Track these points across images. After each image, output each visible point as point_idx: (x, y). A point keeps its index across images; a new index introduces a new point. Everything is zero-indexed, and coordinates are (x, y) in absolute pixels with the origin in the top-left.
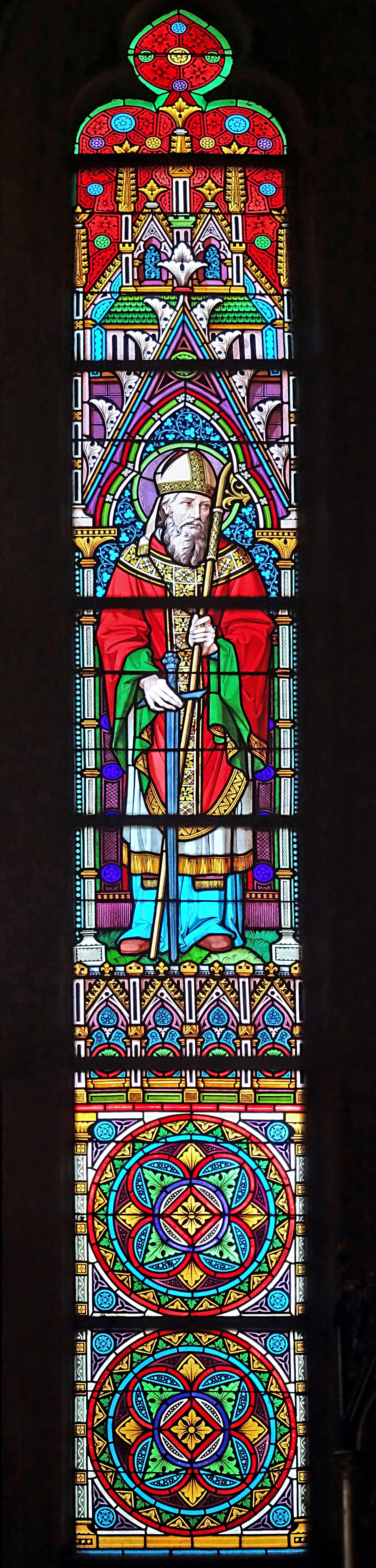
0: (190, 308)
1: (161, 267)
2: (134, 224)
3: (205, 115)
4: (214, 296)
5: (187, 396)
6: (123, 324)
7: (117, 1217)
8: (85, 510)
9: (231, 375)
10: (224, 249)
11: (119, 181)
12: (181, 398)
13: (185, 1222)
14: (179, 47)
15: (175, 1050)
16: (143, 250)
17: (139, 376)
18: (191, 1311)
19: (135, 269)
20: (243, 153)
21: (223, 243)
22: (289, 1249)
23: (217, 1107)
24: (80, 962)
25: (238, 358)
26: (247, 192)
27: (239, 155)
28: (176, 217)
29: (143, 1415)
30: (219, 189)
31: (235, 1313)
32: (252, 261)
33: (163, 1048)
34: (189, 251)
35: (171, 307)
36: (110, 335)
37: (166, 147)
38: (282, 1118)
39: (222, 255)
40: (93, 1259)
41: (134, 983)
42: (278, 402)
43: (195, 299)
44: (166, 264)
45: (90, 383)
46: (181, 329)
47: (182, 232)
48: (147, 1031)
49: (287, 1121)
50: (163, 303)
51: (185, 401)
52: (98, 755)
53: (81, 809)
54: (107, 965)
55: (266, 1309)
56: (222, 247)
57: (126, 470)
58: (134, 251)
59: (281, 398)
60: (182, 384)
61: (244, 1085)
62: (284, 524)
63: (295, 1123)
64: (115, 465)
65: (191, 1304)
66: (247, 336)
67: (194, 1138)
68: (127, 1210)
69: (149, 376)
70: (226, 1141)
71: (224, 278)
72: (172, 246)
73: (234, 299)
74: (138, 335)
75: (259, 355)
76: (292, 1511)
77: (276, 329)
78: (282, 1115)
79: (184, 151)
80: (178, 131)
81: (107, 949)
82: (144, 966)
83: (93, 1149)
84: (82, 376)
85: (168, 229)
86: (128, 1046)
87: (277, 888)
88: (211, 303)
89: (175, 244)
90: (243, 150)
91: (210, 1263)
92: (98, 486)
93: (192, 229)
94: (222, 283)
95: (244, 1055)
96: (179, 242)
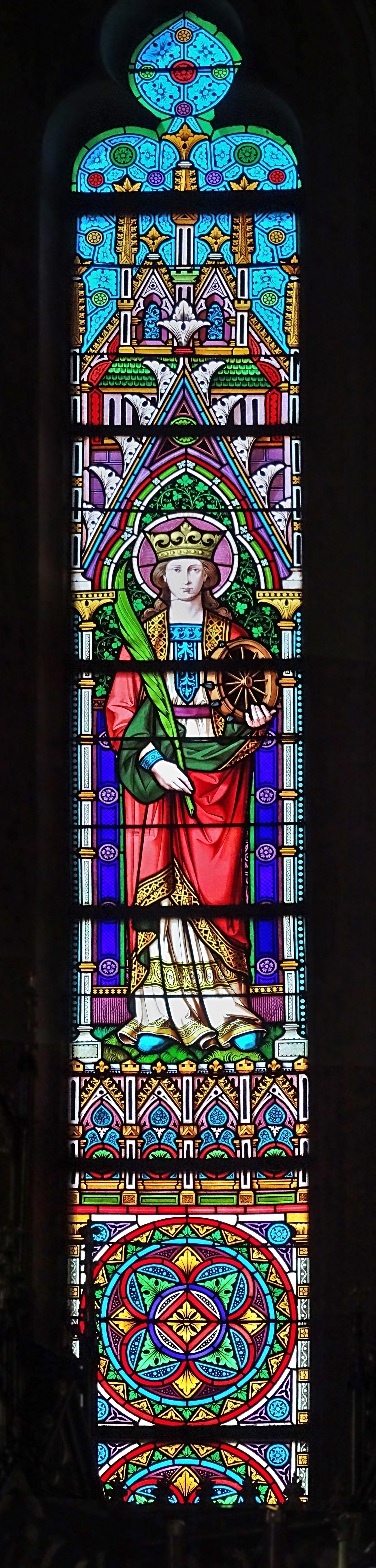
0: (190, 370)
1: (161, 327)
2: (134, 278)
4: (217, 358)
5: (188, 461)
7: (110, 1322)
9: (232, 441)
10: (229, 307)
12: (181, 465)
15: (171, 1151)
16: (142, 307)
17: (140, 442)
18: (186, 1421)
21: (227, 300)
22: (291, 1355)
23: (216, 1210)
24: (77, 1059)
25: (240, 424)
28: (179, 271)
31: (233, 1423)
33: (159, 1149)
34: (191, 309)
35: (171, 370)
38: (283, 1219)
39: (225, 313)
44: (165, 323)
45: (91, 451)
46: (182, 394)
47: (185, 287)
48: (142, 1132)
49: (288, 1221)
50: (163, 366)
51: (186, 467)
54: (102, 1063)
55: (266, 1419)
56: (226, 306)
58: (133, 308)
59: (283, 463)
60: (183, 451)
61: (243, 1187)
62: (285, 584)
63: (296, 1223)
64: (114, 531)
65: (187, 1414)
66: (249, 401)
67: (191, 1241)
68: (120, 1315)
69: (150, 443)
70: (225, 1245)
72: (173, 303)
73: (237, 362)
74: (135, 399)
78: (283, 1215)
79: (189, 189)
84: (83, 442)
85: (170, 284)
86: (123, 1147)
88: (213, 366)
95: (243, 1156)
96: (181, 299)
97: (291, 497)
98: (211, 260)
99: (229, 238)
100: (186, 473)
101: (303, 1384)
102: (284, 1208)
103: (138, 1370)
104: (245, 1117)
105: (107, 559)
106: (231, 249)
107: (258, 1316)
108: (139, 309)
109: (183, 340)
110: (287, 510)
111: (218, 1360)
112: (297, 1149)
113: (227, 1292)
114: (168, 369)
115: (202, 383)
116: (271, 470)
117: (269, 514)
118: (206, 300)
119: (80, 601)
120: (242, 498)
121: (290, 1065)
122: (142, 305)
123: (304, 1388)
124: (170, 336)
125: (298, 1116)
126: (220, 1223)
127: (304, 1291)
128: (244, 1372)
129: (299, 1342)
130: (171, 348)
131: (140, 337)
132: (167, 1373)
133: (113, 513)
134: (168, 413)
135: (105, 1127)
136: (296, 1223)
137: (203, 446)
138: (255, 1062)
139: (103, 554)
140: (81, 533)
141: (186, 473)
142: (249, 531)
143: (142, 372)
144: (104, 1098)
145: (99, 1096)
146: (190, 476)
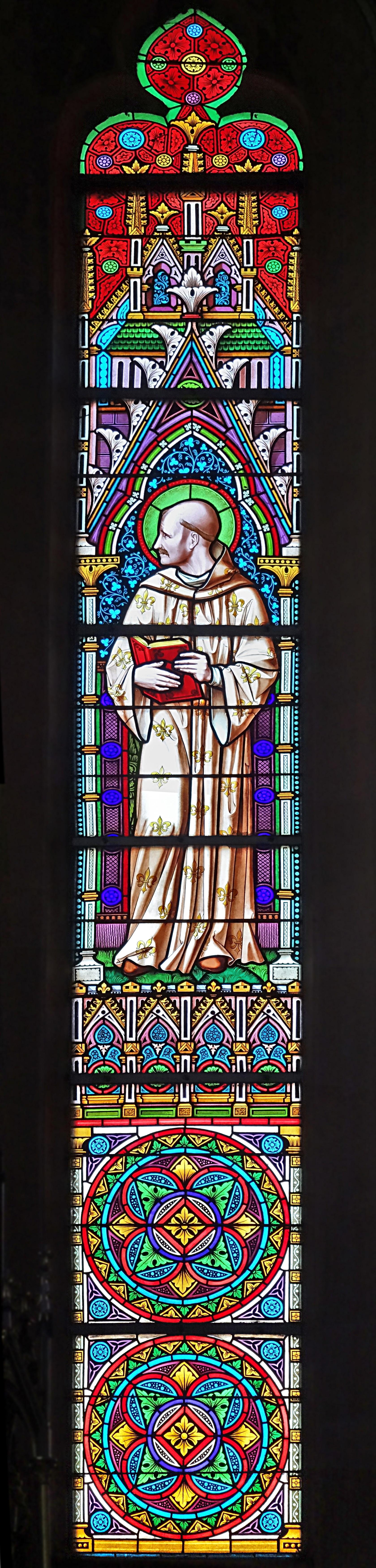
0: (198, 335)
2: (143, 248)
3: (219, 131)
5: (194, 424)
6: (129, 350)
7: (111, 1227)
8: (88, 540)
9: (237, 404)
11: (129, 204)
12: (188, 427)
13: (177, 1233)
14: (194, 53)
16: (151, 275)
17: (147, 405)
19: (144, 294)
20: (257, 171)
21: (234, 268)
24: (80, 982)
26: (259, 216)
27: (254, 173)
29: (130, 1260)
30: (232, 213)
32: (262, 285)
34: (199, 277)
35: (180, 333)
36: (116, 361)
37: (178, 164)
38: (277, 1131)
40: (87, 1269)
41: (131, 1002)
42: (282, 430)
43: (204, 325)
44: (175, 290)
47: (193, 256)
50: (171, 330)
51: (192, 430)
52: (99, 782)
53: (82, 831)
54: (104, 985)
56: (233, 272)
57: (131, 499)
59: (285, 427)
60: (188, 413)
62: (285, 551)
63: (289, 1136)
66: (254, 362)
69: (157, 405)
71: (233, 304)
74: (145, 362)
75: (265, 386)
76: (282, 1516)
77: (285, 356)
78: (277, 1128)
79: (196, 171)
80: (190, 147)
81: (105, 969)
82: (141, 985)
83: (88, 1163)
85: (178, 252)
87: (277, 909)
88: (221, 329)
89: (185, 267)
90: (257, 168)
91: (202, 1271)
92: (103, 514)
93: (203, 253)
94: (232, 310)
96: (189, 267)
97: (292, 463)
98: (218, 232)
99: (235, 213)
100: (192, 436)
101: (295, 1285)
102: (278, 1122)
103: (137, 1270)
104: (241, 1035)
105: (112, 524)
106: (237, 222)
107: (252, 1220)
108: (148, 276)
109: (192, 305)
110: (288, 474)
111: (213, 1262)
112: (289, 1065)
113: (223, 1198)
114: (176, 332)
115: (209, 347)
116: (273, 434)
117: (272, 479)
118: (214, 268)
119: (85, 566)
120: (246, 463)
121: (284, 988)
122: (151, 272)
123: (295, 1289)
124: (180, 302)
125: (291, 1036)
126: (216, 1133)
127: (296, 1199)
128: (238, 1273)
129: (292, 1246)
130: (180, 314)
131: (150, 304)
132: (164, 1273)
133: (119, 479)
134: (175, 376)
135: (107, 1044)
136: (289, 1136)
137: (209, 409)
138: (251, 985)
139: (108, 517)
140: (86, 498)
141: (192, 436)
142: (251, 496)
143: (150, 336)
144: (107, 1017)
145: (101, 1015)
146: (195, 438)
